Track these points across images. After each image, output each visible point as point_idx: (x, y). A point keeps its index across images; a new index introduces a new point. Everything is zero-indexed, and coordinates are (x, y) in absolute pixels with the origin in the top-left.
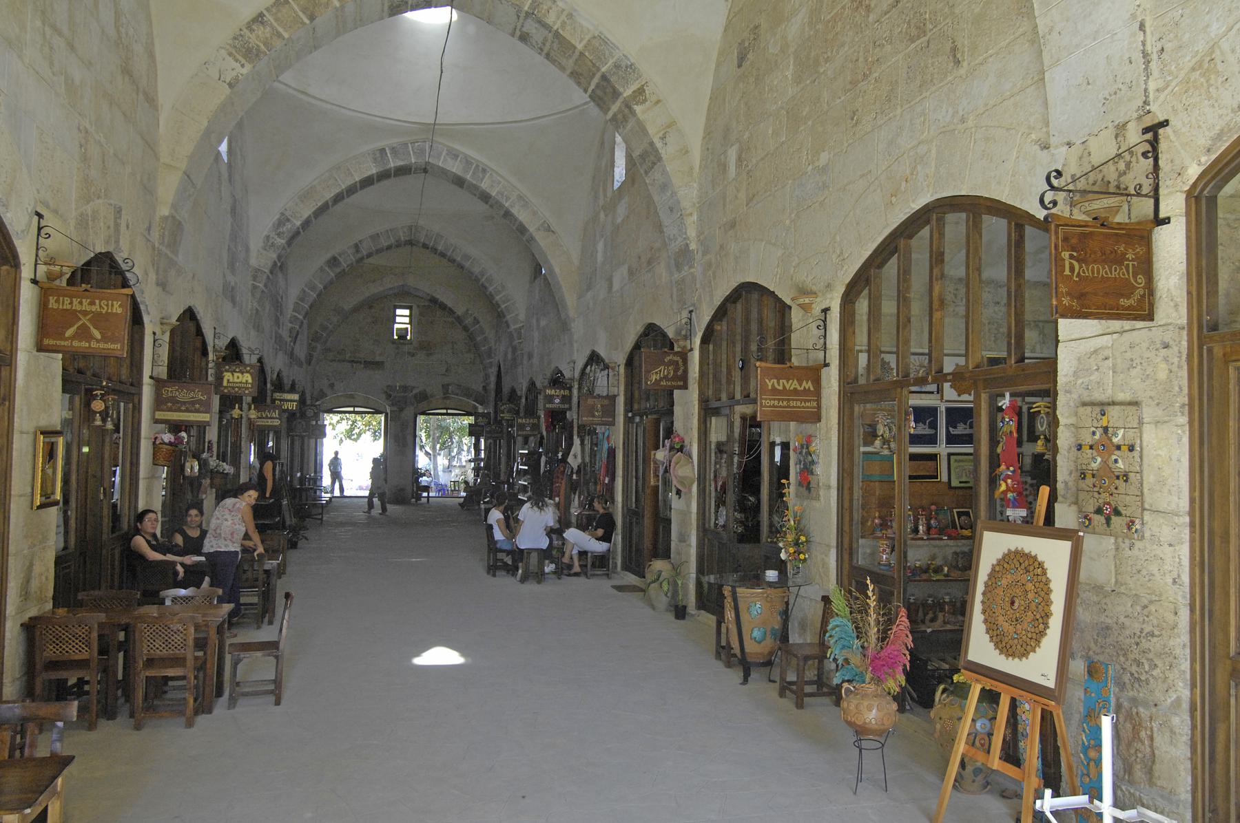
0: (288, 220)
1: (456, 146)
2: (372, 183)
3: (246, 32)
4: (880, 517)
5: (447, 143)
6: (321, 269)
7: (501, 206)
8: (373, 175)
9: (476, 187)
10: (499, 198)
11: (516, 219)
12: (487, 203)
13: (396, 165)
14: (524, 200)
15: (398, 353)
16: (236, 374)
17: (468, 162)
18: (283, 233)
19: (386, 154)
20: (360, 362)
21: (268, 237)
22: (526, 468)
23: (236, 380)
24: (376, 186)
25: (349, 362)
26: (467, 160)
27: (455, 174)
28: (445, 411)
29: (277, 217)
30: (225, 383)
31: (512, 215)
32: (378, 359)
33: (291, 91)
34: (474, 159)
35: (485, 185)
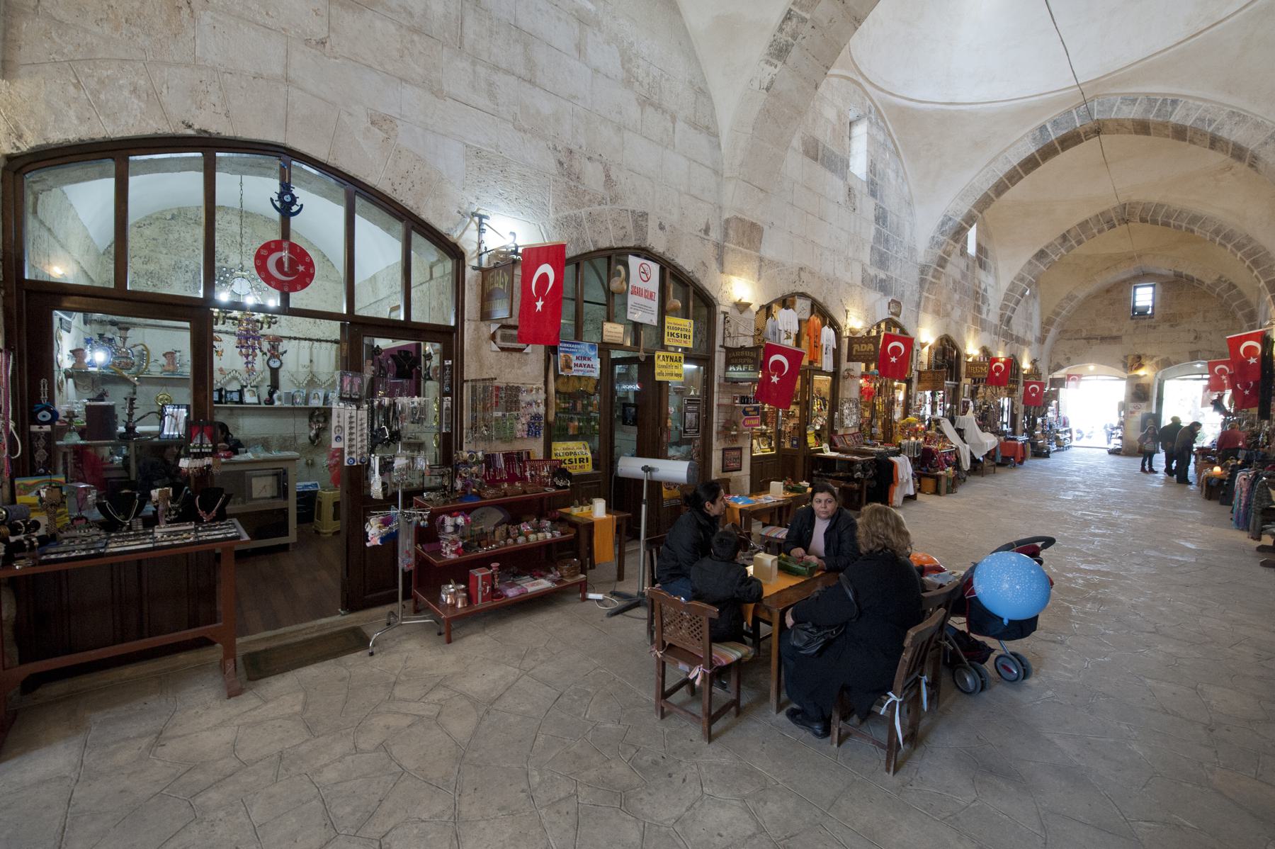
0: (950, 219)
1: (1133, 90)
2: (1037, 165)
3: (778, 35)
4: (821, 426)
5: (1118, 91)
6: (1030, 262)
7: (1204, 134)
8: (1033, 154)
9: (1165, 125)
10: (1199, 125)
11: (1227, 143)
12: (1184, 140)
13: (1057, 136)
14: (1239, 115)
15: (1137, 327)
16: (862, 345)
17: (1150, 100)
18: (946, 231)
19: (1047, 129)
20: (1097, 339)
21: (933, 238)
22: (799, 377)
23: (862, 350)
24: (1044, 167)
25: (1085, 339)
26: (1149, 99)
27: (1133, 120)
28: (1200, 376)
29: (941, 219)
30: (854, 353)
31: (1221, 139)
32: (1115, 333)
33: (938, 106)
34: (1157, 94)
35: (1177, 117)
